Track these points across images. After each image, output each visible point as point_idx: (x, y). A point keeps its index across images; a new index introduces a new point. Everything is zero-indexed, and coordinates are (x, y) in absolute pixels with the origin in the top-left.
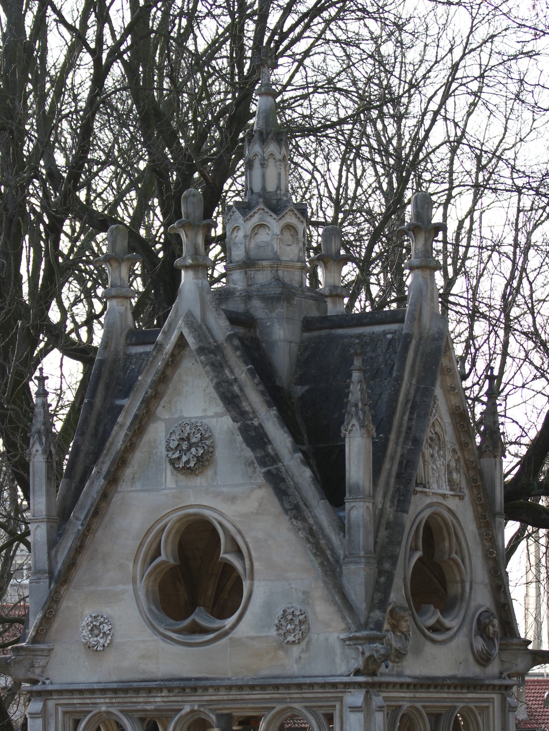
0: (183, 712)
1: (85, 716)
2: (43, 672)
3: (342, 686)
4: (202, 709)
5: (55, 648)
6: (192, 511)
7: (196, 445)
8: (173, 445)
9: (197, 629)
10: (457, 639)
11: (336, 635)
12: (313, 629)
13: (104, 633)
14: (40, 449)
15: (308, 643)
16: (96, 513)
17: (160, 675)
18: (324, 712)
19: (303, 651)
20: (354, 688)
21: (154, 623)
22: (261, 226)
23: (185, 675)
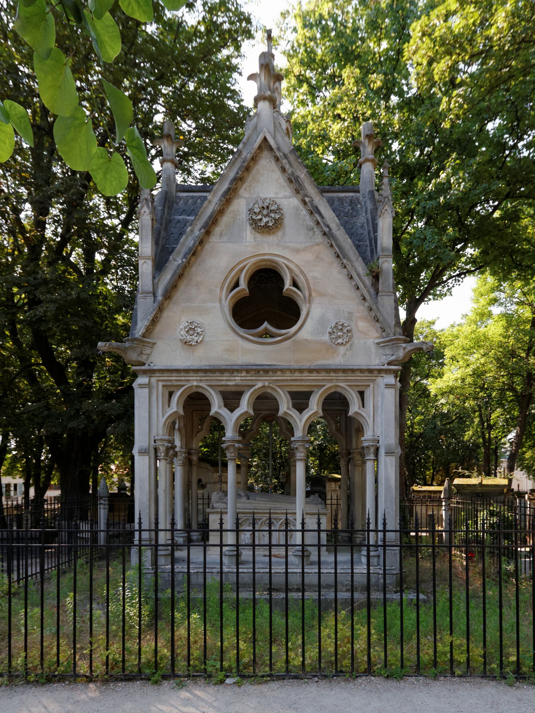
0: (257, 387)
1: (178, 390)
2: (148, 358)
3: (376, 372)
4: (271, 385)
5: (158, 343)
6: (266, 257)
8: (257, 210)
9: (267, 334)
11: (372, 340)
12: (355, 336)
13: (198, 333)
14: (148, 211)
15: (351, 345)
16: (193, 254)
17: (240, 362)
18: (289, 390)
19: (347, 350)
20: (386, 373)
21: (235, 328)
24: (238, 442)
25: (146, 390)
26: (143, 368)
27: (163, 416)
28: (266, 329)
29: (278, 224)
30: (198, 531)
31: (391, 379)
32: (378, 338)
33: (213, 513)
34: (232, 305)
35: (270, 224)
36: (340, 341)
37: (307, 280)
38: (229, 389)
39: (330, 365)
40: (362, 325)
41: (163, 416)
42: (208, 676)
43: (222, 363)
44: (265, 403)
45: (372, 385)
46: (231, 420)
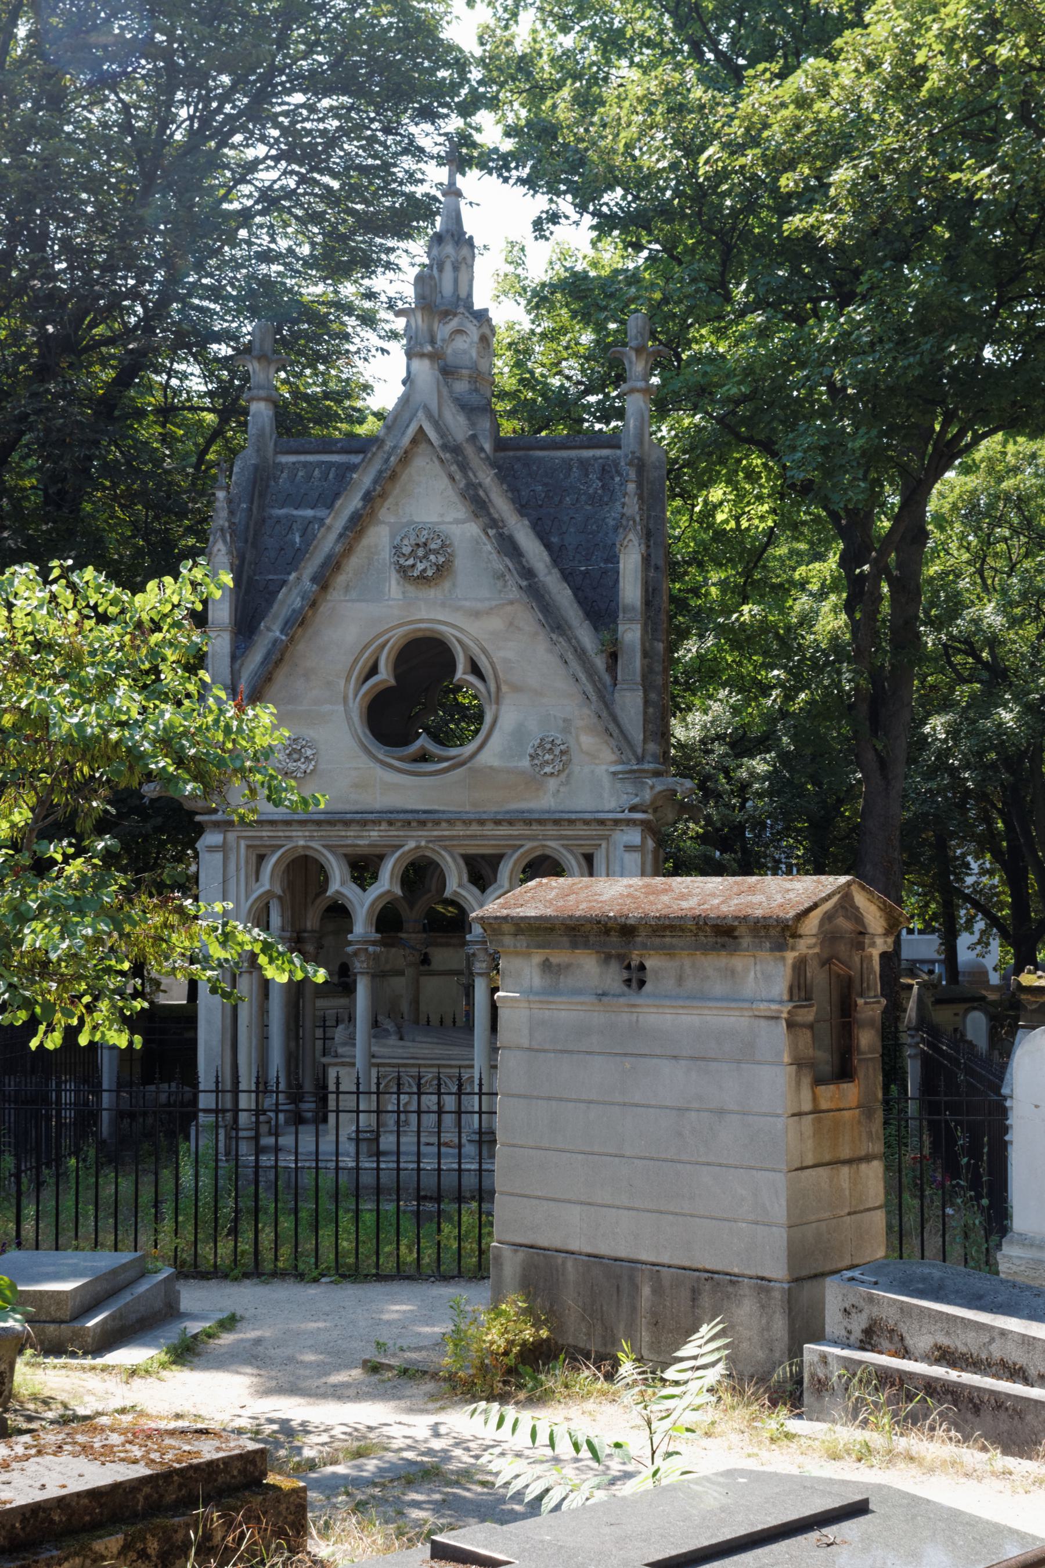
0: (406, 848)
1: (273, 852)
7: (436, 552)
8: (406, 550)
9: (423, 757)
10: (514, 806)
17: (378, 806)
19: (562, 784)
22: (459, 332)
23: (409, 807)
24: (374, 943)
25: (219, 856)
26: (214, 817)
27: (247, 898)
28: (423, 748)
29: (443, 571)
30: (307, 1098)
31: (634, 836)
32: (616, 763)
33: (335, 1065)
34: (365, 705)
35: (430, 573)
36: (548, 769)
37: (492, 664)
38: (359, 851)
39: (529, 811)
40: (587, 741)
41: (247, 898)
42: (300, 1277)
43: (348, 807)
44: (420, 874)
45: (604, 844)
46: (363, 904)
